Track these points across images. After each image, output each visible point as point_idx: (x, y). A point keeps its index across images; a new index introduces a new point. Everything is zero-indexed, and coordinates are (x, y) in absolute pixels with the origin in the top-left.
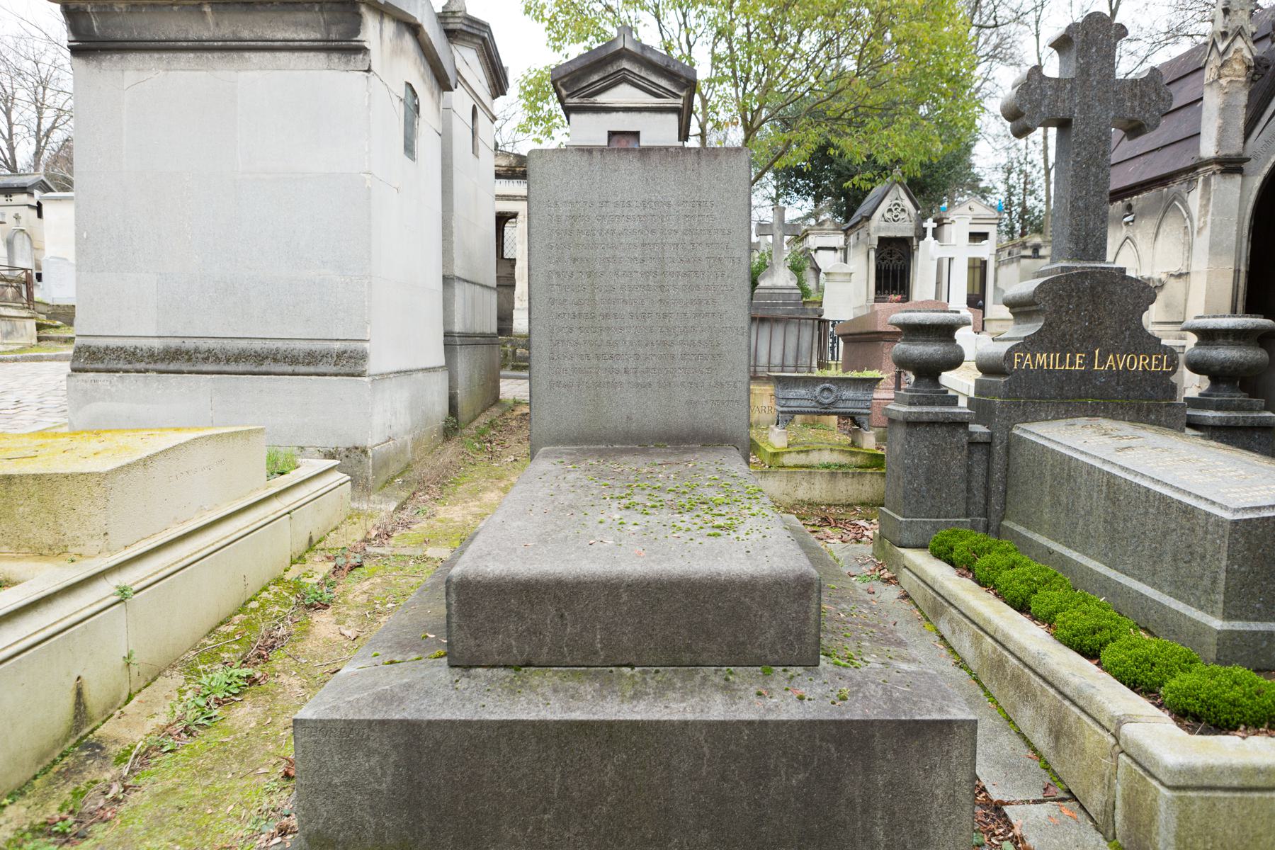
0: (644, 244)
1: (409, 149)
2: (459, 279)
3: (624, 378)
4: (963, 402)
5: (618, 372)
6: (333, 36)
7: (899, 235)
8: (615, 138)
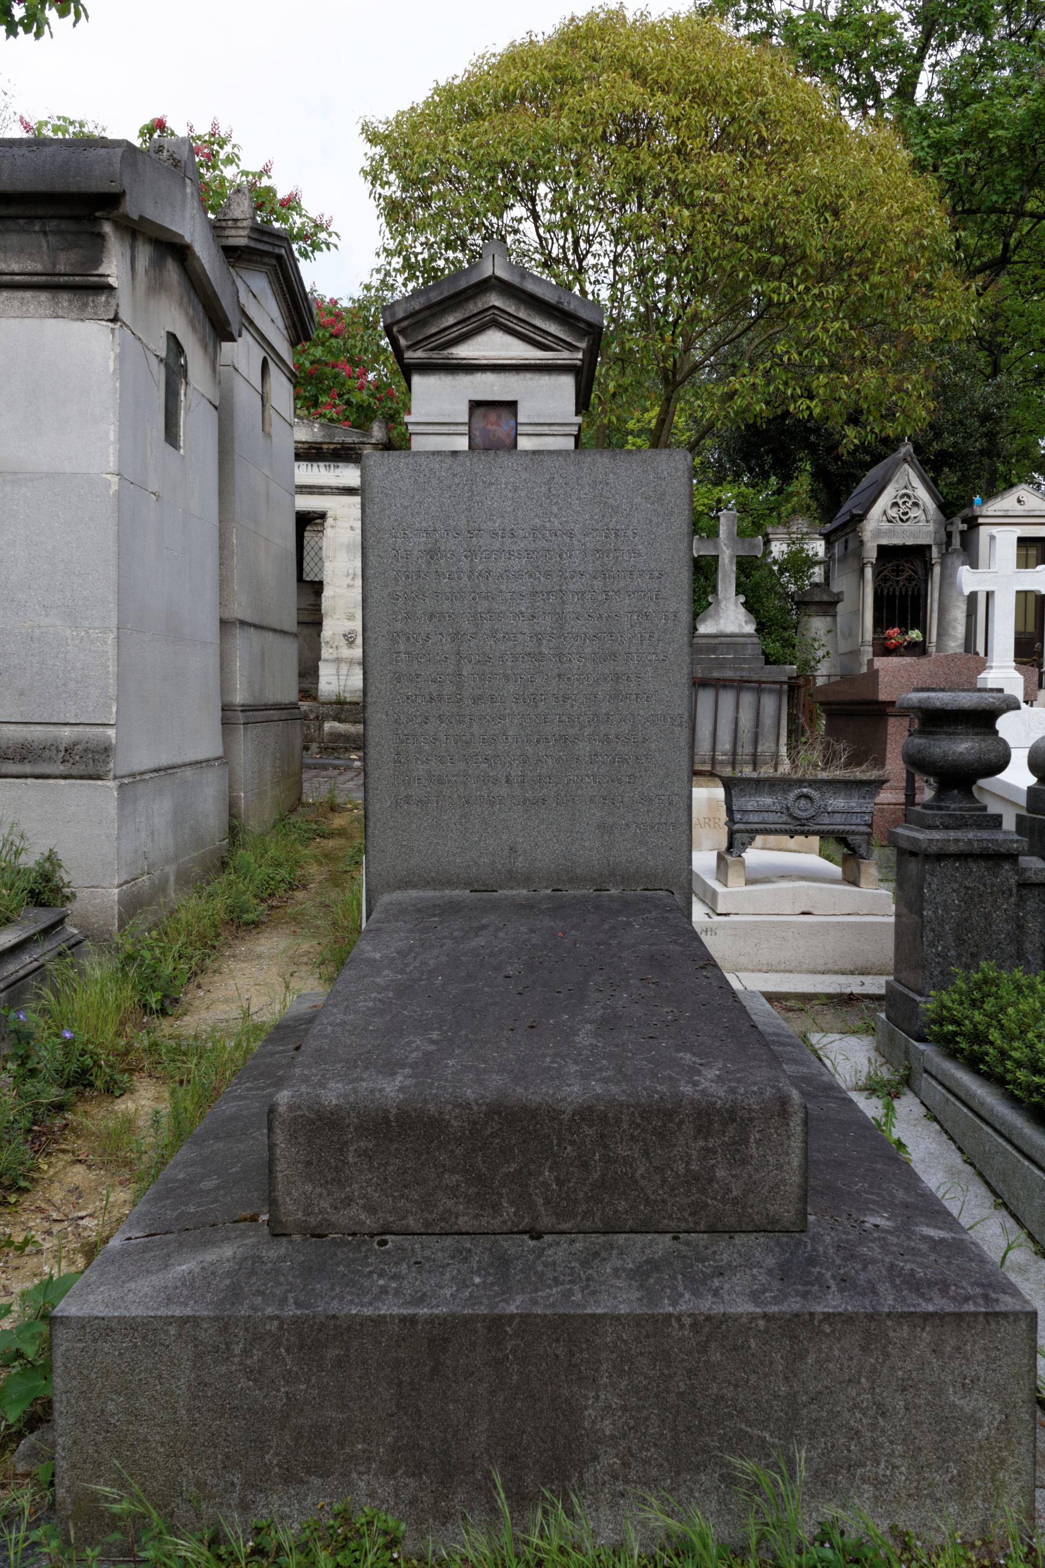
0: (534, 593)
1: (171, 435)
2: (243, 623)
3: (504, 790)
4: (1009, 823)
5: (496, 781)
6: (61, 268)
7: (910, 542)
8: (480, 411)
